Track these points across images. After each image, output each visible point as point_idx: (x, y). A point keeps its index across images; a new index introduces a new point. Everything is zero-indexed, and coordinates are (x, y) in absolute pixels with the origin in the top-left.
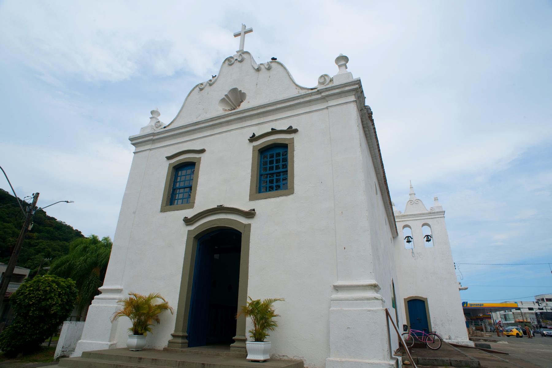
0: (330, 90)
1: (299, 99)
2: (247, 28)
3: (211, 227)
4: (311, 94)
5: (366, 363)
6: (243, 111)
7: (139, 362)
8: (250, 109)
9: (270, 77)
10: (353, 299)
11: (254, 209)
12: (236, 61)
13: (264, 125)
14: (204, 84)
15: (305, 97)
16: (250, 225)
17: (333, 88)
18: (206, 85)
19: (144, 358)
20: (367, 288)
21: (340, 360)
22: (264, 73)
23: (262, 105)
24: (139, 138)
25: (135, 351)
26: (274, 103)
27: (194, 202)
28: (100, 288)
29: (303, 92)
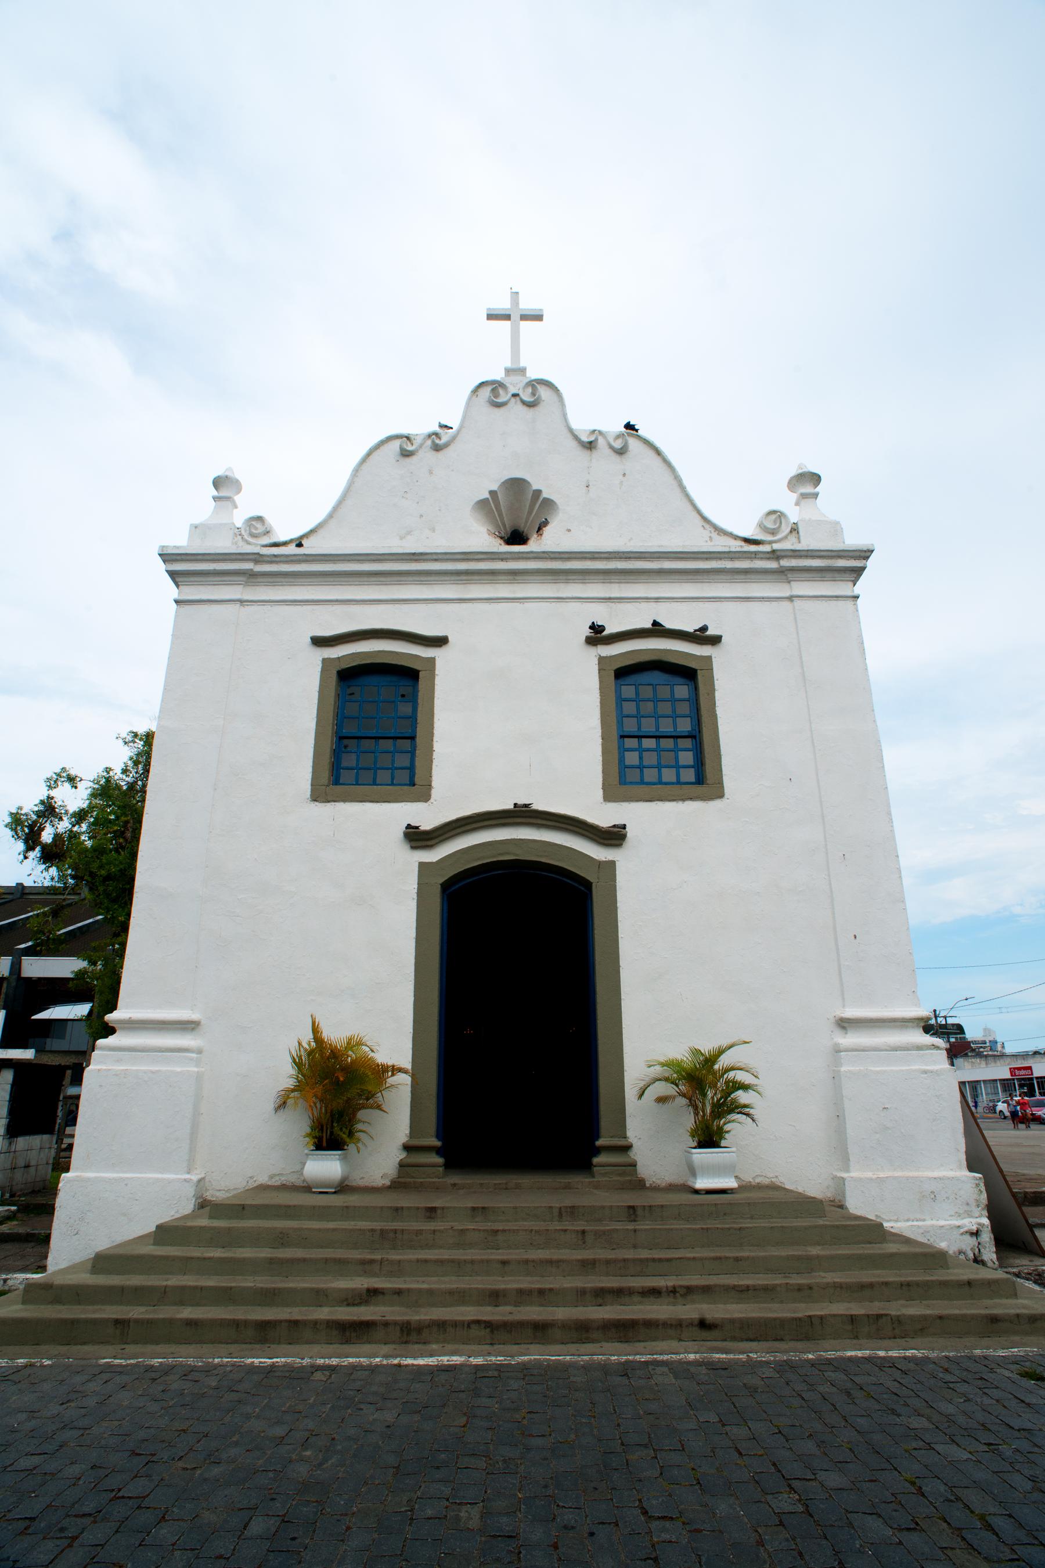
0: (800, 557)
1: (721, 559)
2: (527, 304)
3: (495, 860)
4: (753, 556)
5: (930, 1178)
6: (567, 556)
7: (430, 1217)
8: (587, 555)
9: (624, 475)
10: (887, 1048)
11: (625, 825)
12: (513, 400)
13: (622, 604)
14: (417, 442)
15: (738, 558)
16: (612, 864)
17: (809, 553)
18: (421, 446)
19: (443, 1208)
20: (911, 1024)
21: (876, 1176)
22: (603, 461)
23: (623, 553)
24: (200, 557)
25: (335, 1193)
26: (657, 555)
27: (430, 785)
28: (109, 1017)
29: (721, 544)
